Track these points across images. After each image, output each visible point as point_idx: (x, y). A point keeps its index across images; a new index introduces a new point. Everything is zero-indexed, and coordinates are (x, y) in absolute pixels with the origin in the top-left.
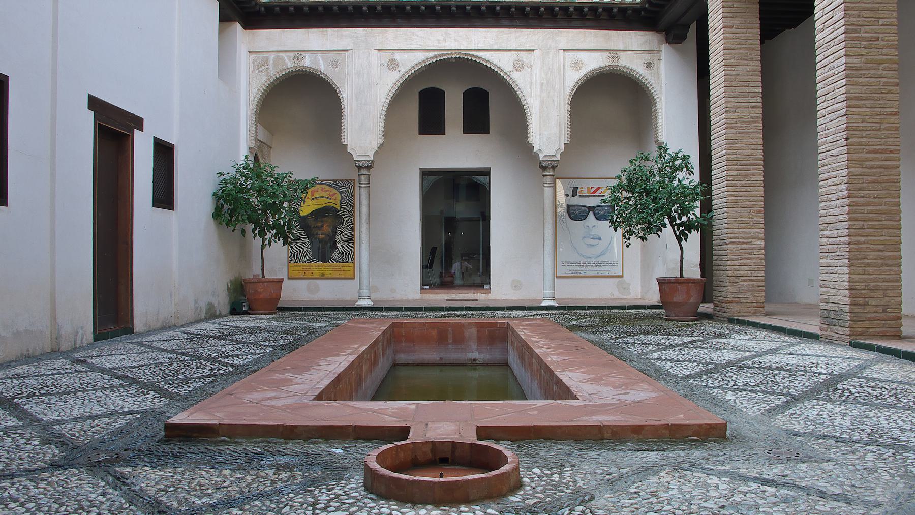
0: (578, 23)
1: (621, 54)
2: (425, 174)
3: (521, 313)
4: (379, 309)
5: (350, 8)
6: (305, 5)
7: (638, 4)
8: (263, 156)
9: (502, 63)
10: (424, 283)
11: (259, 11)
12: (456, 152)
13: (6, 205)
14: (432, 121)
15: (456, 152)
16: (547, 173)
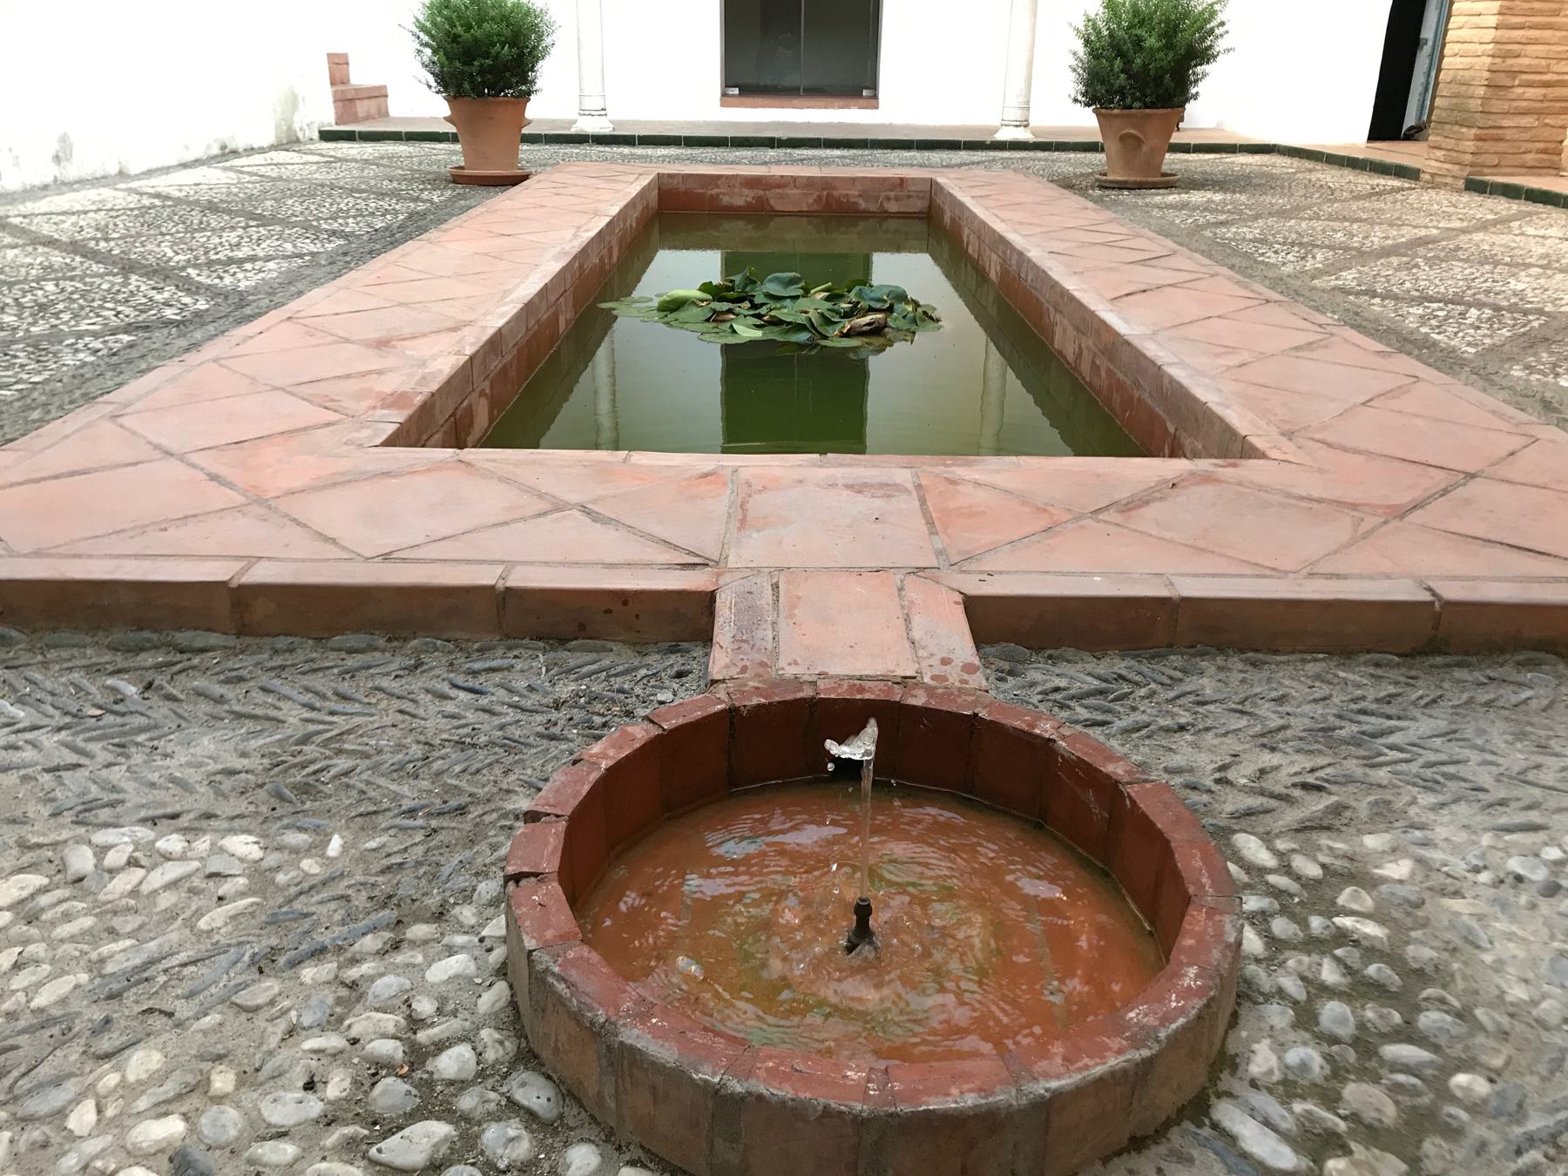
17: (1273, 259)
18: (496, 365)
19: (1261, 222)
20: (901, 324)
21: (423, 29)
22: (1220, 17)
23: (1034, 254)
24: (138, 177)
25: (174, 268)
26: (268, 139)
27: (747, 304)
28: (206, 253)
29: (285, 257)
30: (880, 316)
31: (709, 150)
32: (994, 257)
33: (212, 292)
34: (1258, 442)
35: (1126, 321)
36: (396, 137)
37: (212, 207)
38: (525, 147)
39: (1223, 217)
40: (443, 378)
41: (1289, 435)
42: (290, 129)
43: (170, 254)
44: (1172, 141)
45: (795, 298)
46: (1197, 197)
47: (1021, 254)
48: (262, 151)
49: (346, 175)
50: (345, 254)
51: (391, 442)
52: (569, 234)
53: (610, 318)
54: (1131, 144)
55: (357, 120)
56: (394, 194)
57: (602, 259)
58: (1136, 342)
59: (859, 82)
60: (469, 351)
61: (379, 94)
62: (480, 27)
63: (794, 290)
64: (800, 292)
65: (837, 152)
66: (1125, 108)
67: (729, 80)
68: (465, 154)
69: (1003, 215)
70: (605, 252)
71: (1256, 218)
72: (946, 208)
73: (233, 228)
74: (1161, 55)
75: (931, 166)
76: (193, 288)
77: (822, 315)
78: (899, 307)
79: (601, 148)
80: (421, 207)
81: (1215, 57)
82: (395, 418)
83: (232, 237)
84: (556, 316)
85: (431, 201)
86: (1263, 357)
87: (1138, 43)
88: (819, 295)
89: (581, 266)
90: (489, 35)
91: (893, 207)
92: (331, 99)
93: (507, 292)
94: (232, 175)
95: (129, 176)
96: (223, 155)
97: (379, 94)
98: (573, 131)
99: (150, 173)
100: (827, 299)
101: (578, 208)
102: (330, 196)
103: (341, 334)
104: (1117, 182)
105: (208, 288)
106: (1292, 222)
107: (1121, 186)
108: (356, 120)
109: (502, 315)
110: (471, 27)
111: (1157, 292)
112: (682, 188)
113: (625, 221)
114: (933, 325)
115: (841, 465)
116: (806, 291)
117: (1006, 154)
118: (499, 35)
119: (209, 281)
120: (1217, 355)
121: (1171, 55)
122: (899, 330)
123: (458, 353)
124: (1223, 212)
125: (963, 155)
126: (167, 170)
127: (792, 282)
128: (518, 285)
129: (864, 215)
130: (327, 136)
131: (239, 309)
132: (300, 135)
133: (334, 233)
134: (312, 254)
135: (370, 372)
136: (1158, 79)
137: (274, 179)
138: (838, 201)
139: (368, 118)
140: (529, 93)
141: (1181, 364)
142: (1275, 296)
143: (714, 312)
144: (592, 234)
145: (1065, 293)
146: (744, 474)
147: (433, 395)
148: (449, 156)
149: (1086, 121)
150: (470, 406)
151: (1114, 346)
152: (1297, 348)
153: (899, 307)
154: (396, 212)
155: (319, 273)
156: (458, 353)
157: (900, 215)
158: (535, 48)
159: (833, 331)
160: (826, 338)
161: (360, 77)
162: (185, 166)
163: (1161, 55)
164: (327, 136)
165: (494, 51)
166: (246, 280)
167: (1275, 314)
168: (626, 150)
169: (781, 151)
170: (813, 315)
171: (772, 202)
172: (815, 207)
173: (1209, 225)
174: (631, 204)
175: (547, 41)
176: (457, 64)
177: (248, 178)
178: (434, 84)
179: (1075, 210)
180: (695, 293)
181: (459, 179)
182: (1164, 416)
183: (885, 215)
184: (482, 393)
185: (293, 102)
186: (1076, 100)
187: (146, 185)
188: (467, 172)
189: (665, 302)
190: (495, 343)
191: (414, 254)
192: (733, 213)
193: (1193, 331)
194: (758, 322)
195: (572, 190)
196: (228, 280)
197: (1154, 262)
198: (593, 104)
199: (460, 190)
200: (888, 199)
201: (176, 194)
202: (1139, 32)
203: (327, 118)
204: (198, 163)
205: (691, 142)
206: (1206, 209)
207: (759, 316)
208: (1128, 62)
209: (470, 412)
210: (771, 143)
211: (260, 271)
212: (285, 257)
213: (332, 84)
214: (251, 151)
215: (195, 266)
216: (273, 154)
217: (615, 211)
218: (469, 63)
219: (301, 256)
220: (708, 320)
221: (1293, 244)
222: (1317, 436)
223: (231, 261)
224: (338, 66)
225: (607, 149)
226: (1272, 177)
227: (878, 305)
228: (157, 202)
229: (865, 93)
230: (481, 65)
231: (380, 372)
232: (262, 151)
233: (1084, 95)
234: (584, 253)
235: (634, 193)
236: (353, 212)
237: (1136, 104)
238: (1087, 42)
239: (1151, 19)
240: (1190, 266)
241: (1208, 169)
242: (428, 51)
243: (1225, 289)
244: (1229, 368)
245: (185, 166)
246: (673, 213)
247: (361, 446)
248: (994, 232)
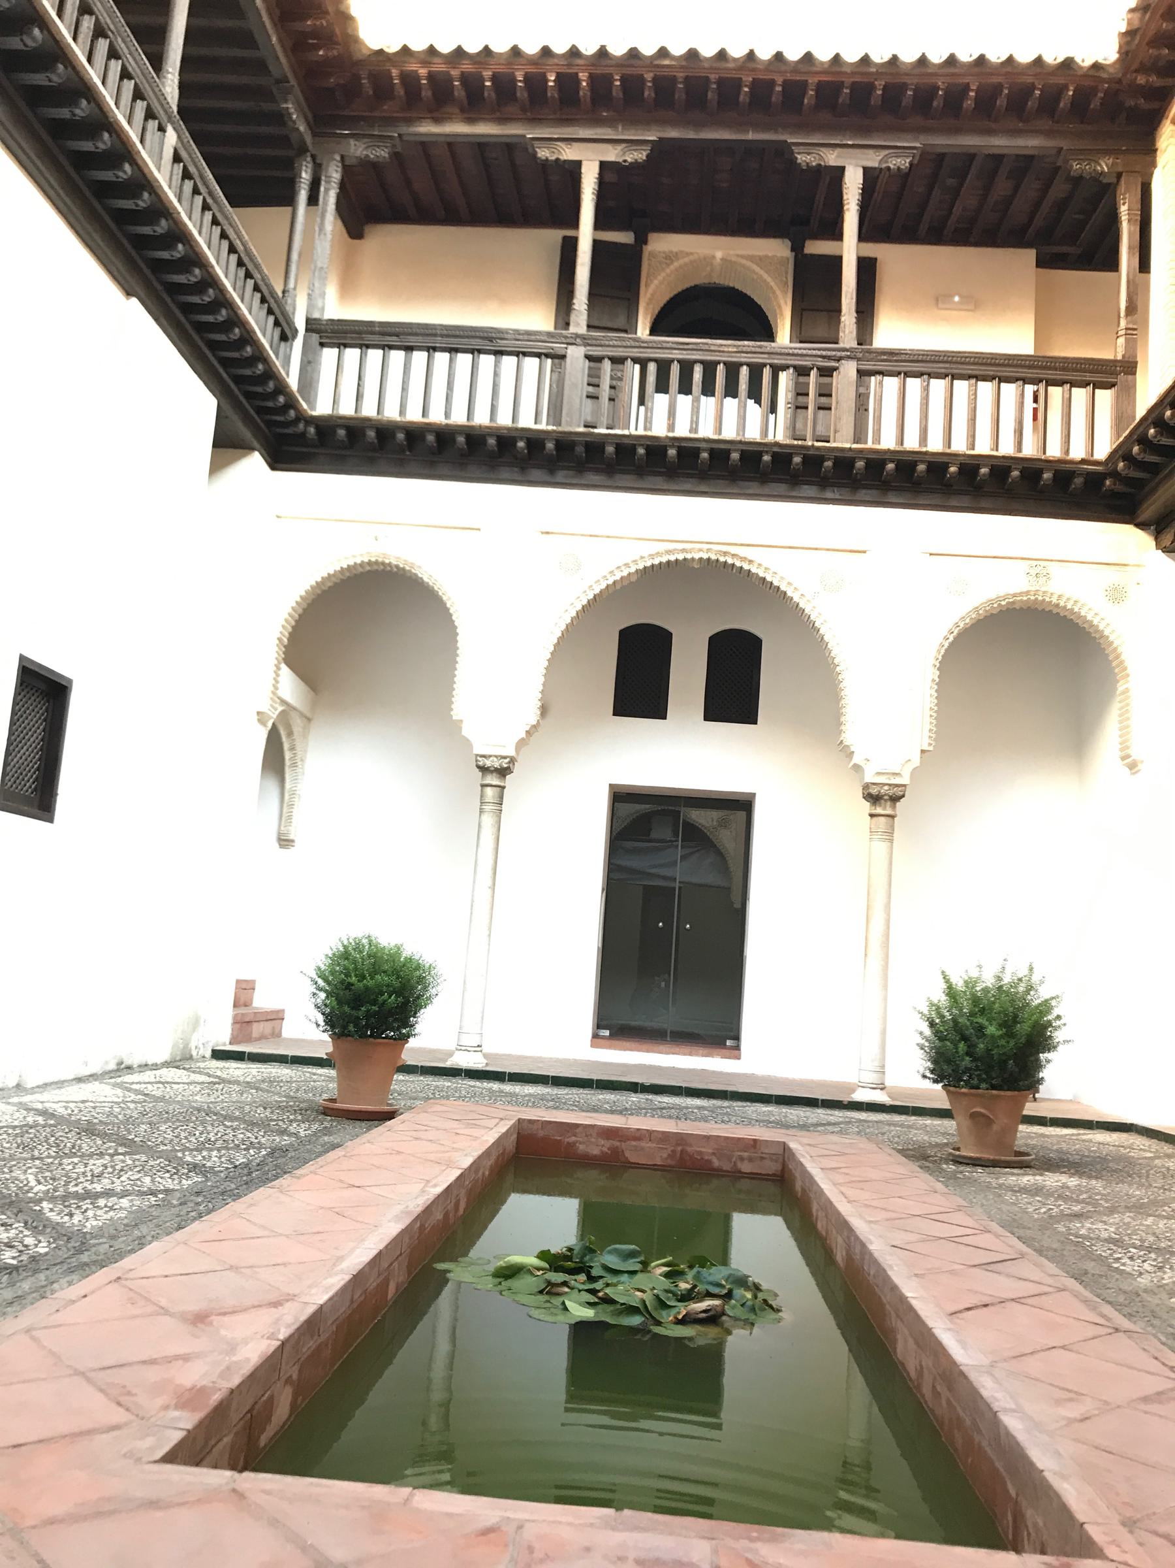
0: (965, 501)
1: (1053, 568)
2: (620, 797)
3: (530, 1089)
4: (498, 1076)
5: (735, 456)
6: (491, 435)
7: (1097, 463)
8: (290, 734)
9: (770, 565)
10: (599, 1024)
11: (303, 434)
12: (684, 754)
13: (51, 820)
14: (640, 687)
15: (684, 754)
16: (879, 810)
17: (1129, 1267)
18: (311, 1344)
19: (1116, 1218)
20: (740, 1312)
21: (321, 975)
22: (1055, 1012)
23: (877, 1246)
24: (33, 1091)
25: (31, 1200)
26: (165, 1056)
27: (582, 1277)
28: (67, 1183)
29: (142, 1194)
30: (717, 1302)
31: (574, 1090)
32: (840, 1240)
33: (60, 1234)
34: (1094, 1532)
35: (963, 1343)
36: (282, 1059)
37: (89, 1130)
38: (399, 1077)
39: (1077, 1208)
40: (247, 1370)
41: (1130, 1524)
42: (186, 1046)
43: (33, 1183)
44: (1025, 1112)
45: (633, 1273)
46: (1052, 1180)
47: (863, 1245)
48: (155, 1067)
49: (224, 1099)
50: (198, 1193)
51: (170, 1458)
52: (416, 1188)
53: (442, 1279)
54: (981, 1122)
55: (251, 1040)
56: (264, 1125)
57: (446, 1215)
58: (973, 1376)
59: (723, 1033)
60: (282, 1335)
61: (276, 1017)
62: (372, 979)
63: (633, 1264)
64: (638, 1267)
65: (698, 1102)
66: (972, 1087)
67: (601, 1021)
68: (341, 1079)
69: (849, 1192)
70: (451, 1207)
71: (1112, 1211)
72: (797, 1175)
73: (101, 1155)
74: (1003, 1042)
75: (787, 1126)
76: (38, 1224)
77: (657, 1296)
78: (739, 1292)
79: (472, 1083)
80: (286, 1140)
81: (1055, 1047)
82: (181, 1423)
83: (96, 1165)
84: (385, 1284)
85: (296, 1135)
86: (1107, 1407)
87: (980, 1029)
88: (659, 1269)
89: (422, 1227)
90: (379, 985)
91: (746, 1167)
92: (230, 1021)
93: (341, 1259)
94: (119, 1092)
95: (25, 1090)
96: (118, 1070)
97: (276, 1017)
98: (448, 1064)
99: (45, 1086)
100: (667, 1275)
101: (432, 1157)
102: (203, 1123)
103: (163, 1302)
104: (971, 1158)
105: (56, 1226)
106: (1150, 1221)
107: (975, 1163)
108: (249, 1039)
109: (327, 1289)
110: (364, 977)
111: (998, 1308)
112: (541, 1133)
113: (477, 1172)
114: (773, 1315)
115: (637, 1528)
116: (645, 1264)
117: (863, 1116)
118: (388, 986)
119: (57, 1219)
120: (1059, 1402)
121: (1012, 1043)
122: (736, 1319)
123: (271, 1337)
124: (1078, 1202)
125: (821, 1114)
126: (60, 1084)
127: (632, 1255)
128: (352, 1251)
129: (717, 1173)
130: (218, 1055)
131: (79, 1255)
132: (194, 1053)
133: (195, 1166)
134: (167, 1191)
135: (177, 1357)
136: (1003, 1063)
137: (157, 1099)
138: (691, 1157)
139: (262, 1038)
140: (408, 1036)
141: (1017, 1411)
142: (1126, 1324)
143: (549, 1283)
144: (439, 1190)
145: (903, 1299)
146: (529, 1533)
147: (232, 1391)
148: (325, 1082)
149: (935, 1094)
150: (272, 1398)
151: (952, 1375)
152: (1146, 1399)
153: (739, 1292)
154: (261, 1146)
155: (167, 1214)
156: (271, 1337)
157: (753, 1176)
158: (418, 997)
159: (667, 1317)
160: (659, 1323)
161: (262, 1001)
162: (79, 1080)
163: (1003, 1042)
164: (218, 1055)
165: (381, 999)
166: (91, 1219)
167: (1124, 1349)
168: (495, 1086)
169: (642, 1097)
170: (648, 1297)
171: (627, 1154)
172: (669, 1162)
173: (1063, 1216)
174: (487, 1153)
175: (433, 991)
176: (346, 1009)
177: (133, 1096)
178: (322, 1023)
179: (922, 1191)
180: (532, 1261)
181: (330, 1111)
182: (1004, 1474)
183: (737, 1175)
184: (288, 1381)
185: (195, 1023)
186: (924, 1076)
187: (35, 1100)
188: (338, 1105)
189: (502, 1268)
190: (311, 1325)
191: (263, 1205)
192: (588, 1162)
193: (1032, 1365)
194: (592, 1299)
195: (431, 1135)
196: (76, 1219)
197: (999, 1267)
198: (470, 1040)
199: (328, 1122)
200: (742, 1159)
201: (61, 1111)
202: (980, 1020)
203: (222, 1038)
204: (93, 1077)
205: (558, 1081)
206: (1060, 1197)
207: (593, 1292)
208: (971, 1046)
209: (270, 1404)
210: (634, 1087)
211: (111, 1208)
212: (142, 1194)
213: (235, 1006)
214: (144, 1067)
215: (52, 1199)
216: (164, 1071)
217: (467, 1162)
218: (356, 1008)
219: (153, 1193)
220: (541, 1292)
221: (1150, 1249)
222: (1164, 1528)
223: (88, 1195)
224: (244, 991)
225: (478, 1084)
226: (1130, 1162)
227: (716, 1290)
228: (40, 1120)
229: (729, 1043)
230: (368, 1011)
231: (186, 1358)
232: (155, 1067)
233: (932, 1072)
234: (428, 1210)
235: (492, 1141)
236: (219, 1144)
237: (983, 1085)
238: (932, 1024)
239: (991, 1009)
240: (1036, 1275)
241: (1064, 1146)
242: (323, 995)
243: (1073, 1312)
244: (1070, 1421)
245: (79, 1080)
246: (531, 1158)
247: (139, 1460)
248: (839, 1214)
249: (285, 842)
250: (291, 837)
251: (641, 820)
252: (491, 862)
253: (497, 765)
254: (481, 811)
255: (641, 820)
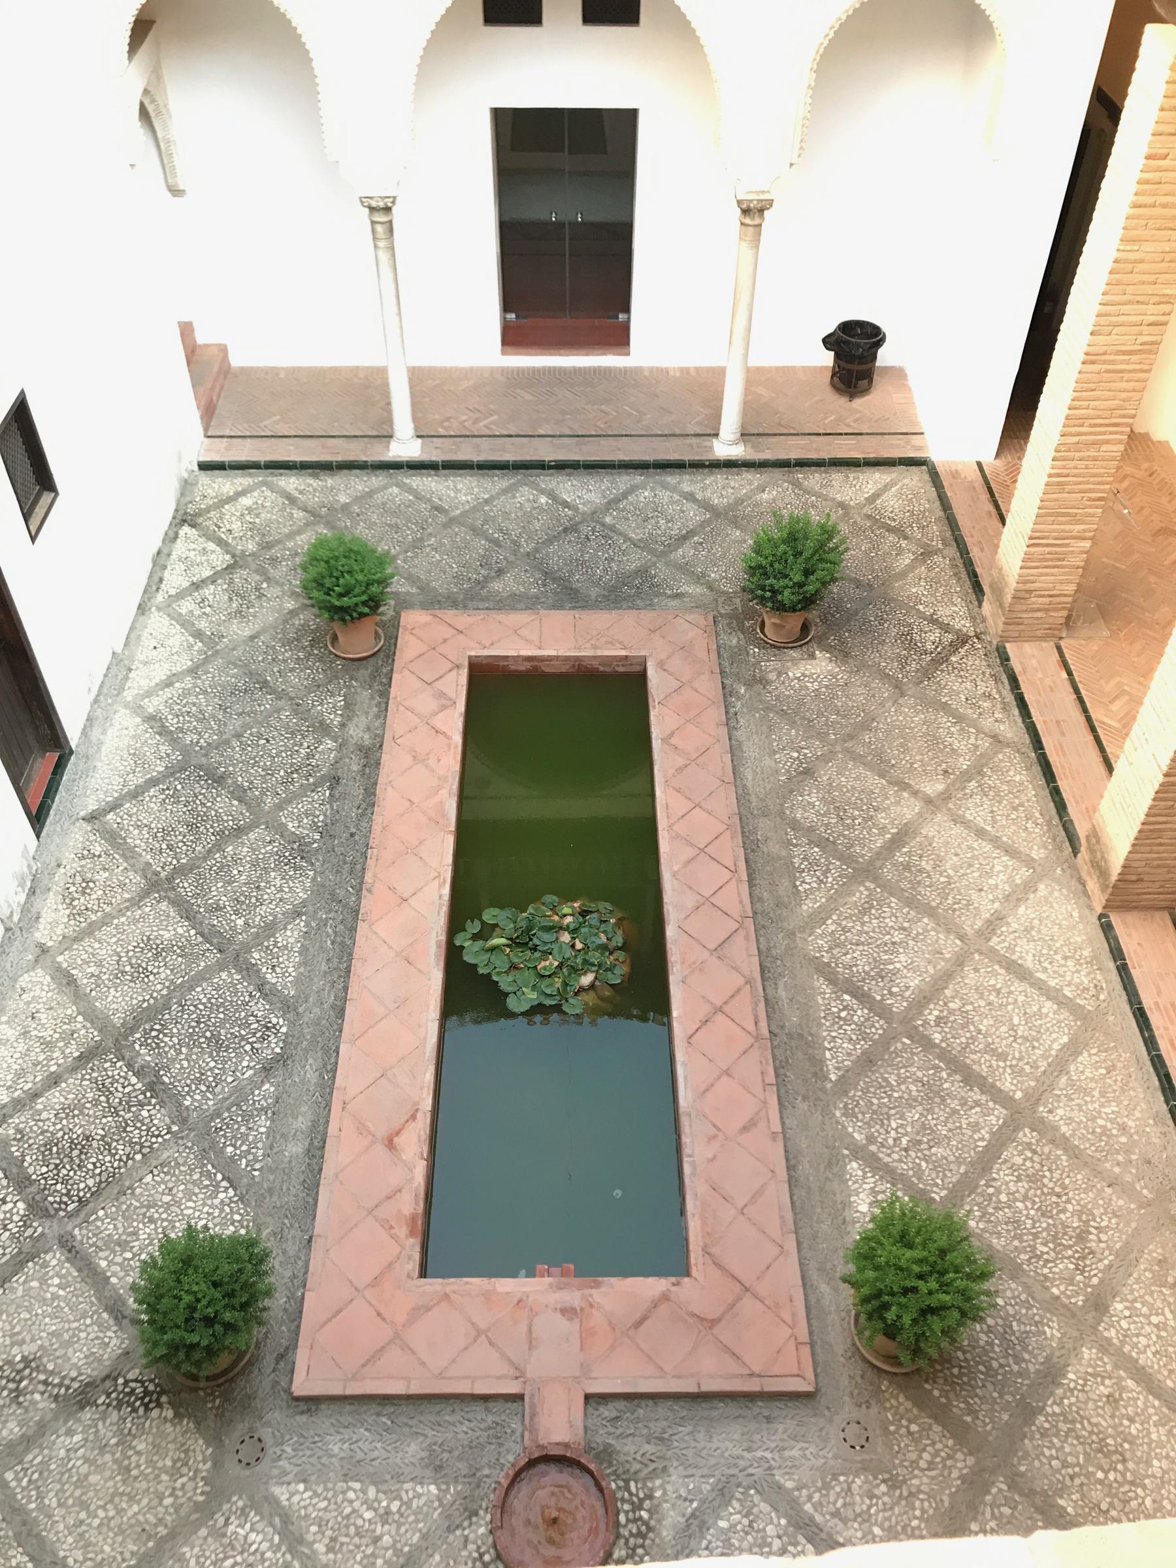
2: (500, 116)
249: (176, 192)
250: (181, 188)
251: (528, 141)
252: (394, 292)
253: (381, 204)
254: (376, 247)
255: (528, 141)
